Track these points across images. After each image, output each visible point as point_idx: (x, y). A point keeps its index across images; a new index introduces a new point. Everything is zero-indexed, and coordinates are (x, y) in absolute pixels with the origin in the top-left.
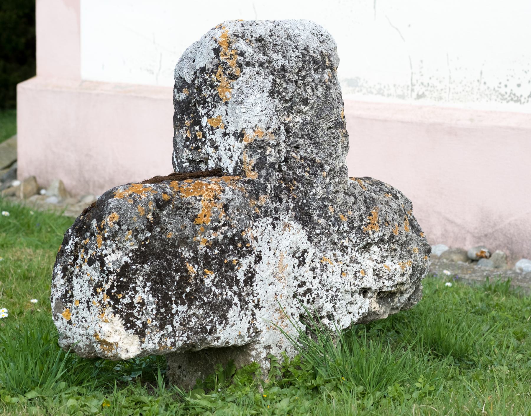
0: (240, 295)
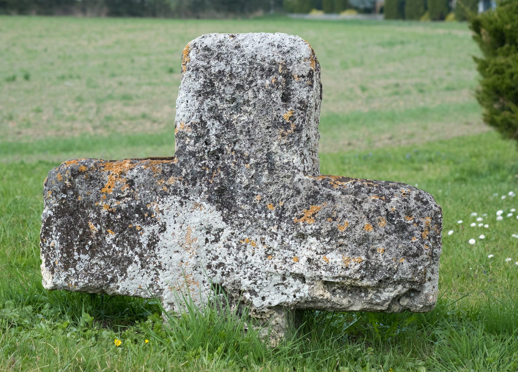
0: (141, 256)
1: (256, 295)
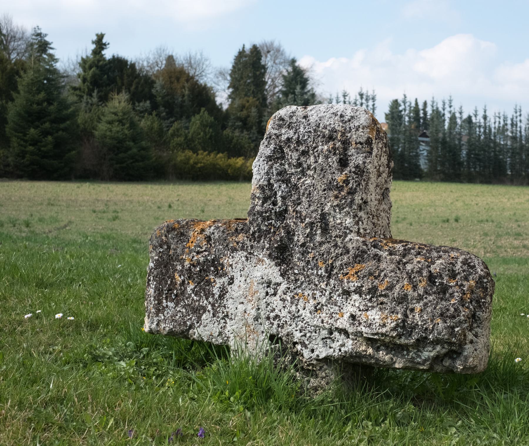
0: (213, 305)
1: (306, 347)
